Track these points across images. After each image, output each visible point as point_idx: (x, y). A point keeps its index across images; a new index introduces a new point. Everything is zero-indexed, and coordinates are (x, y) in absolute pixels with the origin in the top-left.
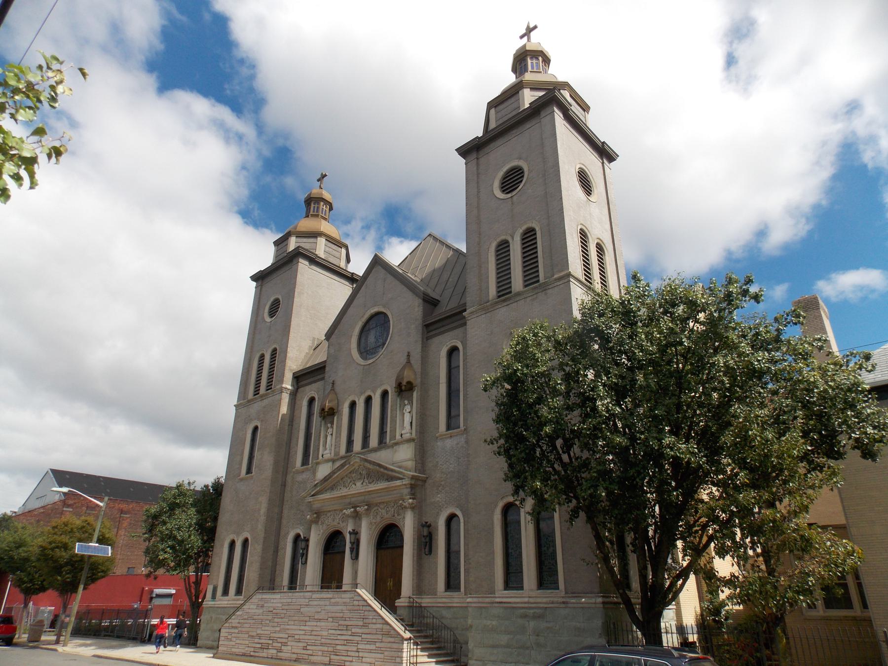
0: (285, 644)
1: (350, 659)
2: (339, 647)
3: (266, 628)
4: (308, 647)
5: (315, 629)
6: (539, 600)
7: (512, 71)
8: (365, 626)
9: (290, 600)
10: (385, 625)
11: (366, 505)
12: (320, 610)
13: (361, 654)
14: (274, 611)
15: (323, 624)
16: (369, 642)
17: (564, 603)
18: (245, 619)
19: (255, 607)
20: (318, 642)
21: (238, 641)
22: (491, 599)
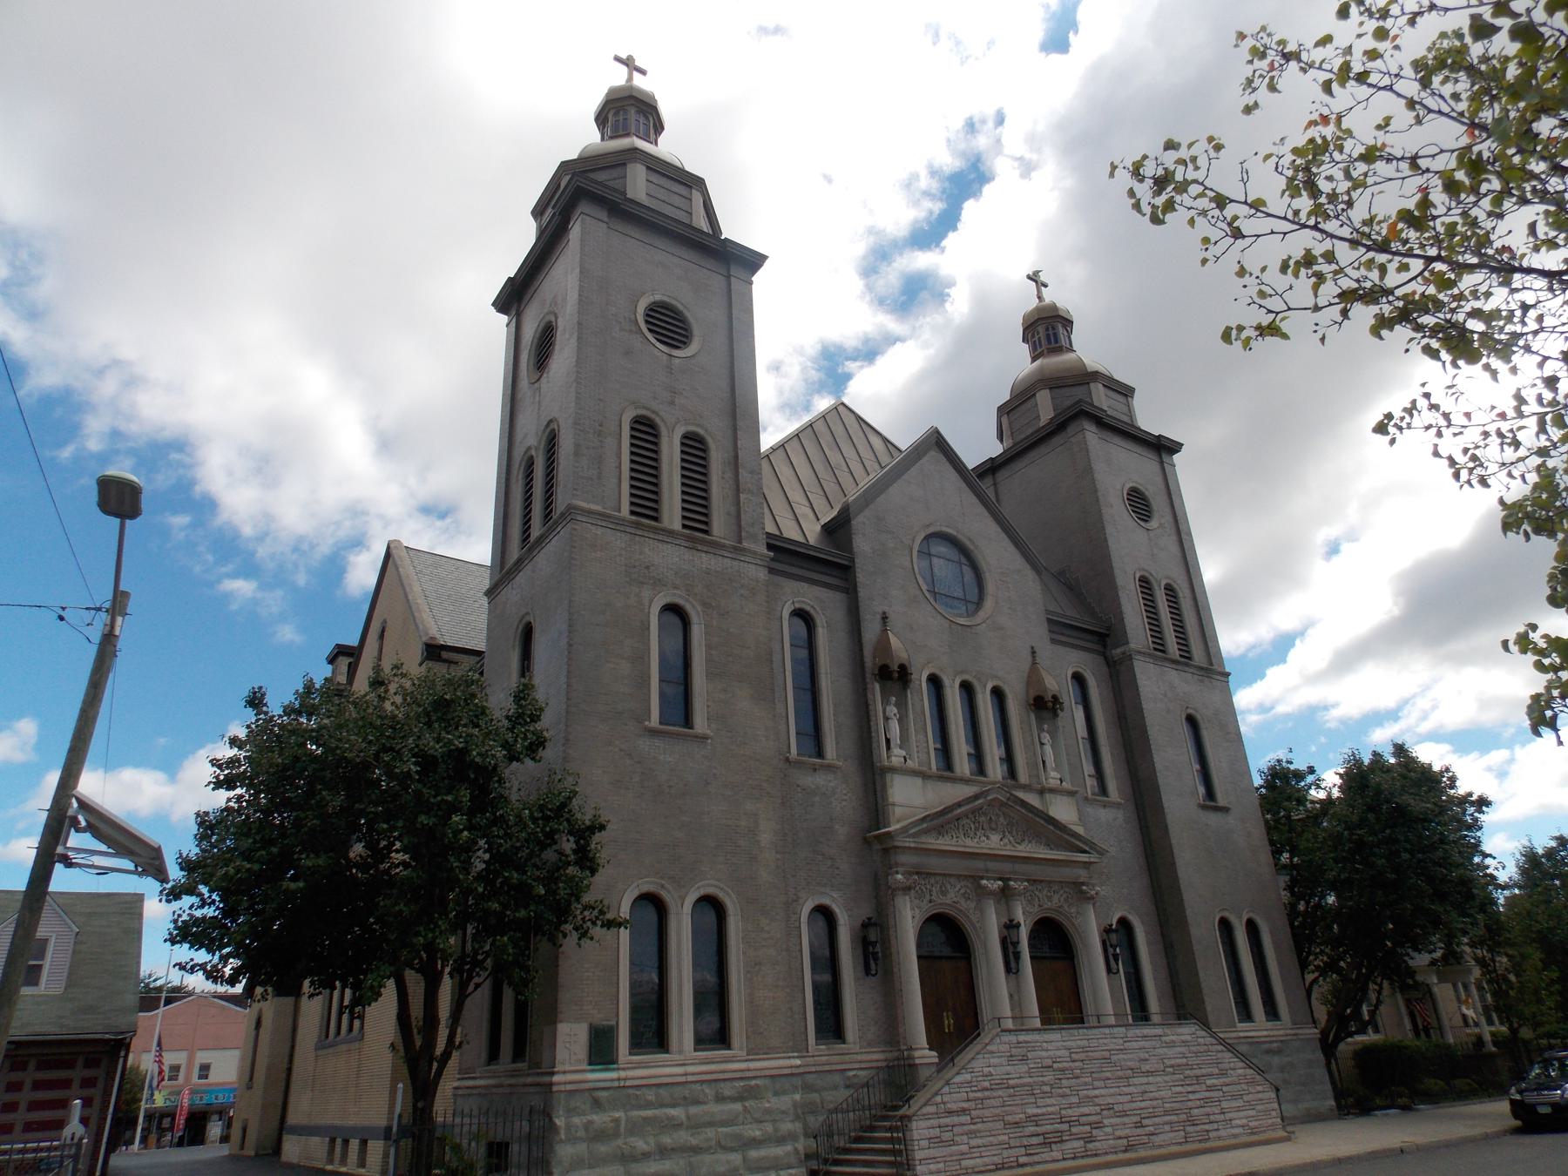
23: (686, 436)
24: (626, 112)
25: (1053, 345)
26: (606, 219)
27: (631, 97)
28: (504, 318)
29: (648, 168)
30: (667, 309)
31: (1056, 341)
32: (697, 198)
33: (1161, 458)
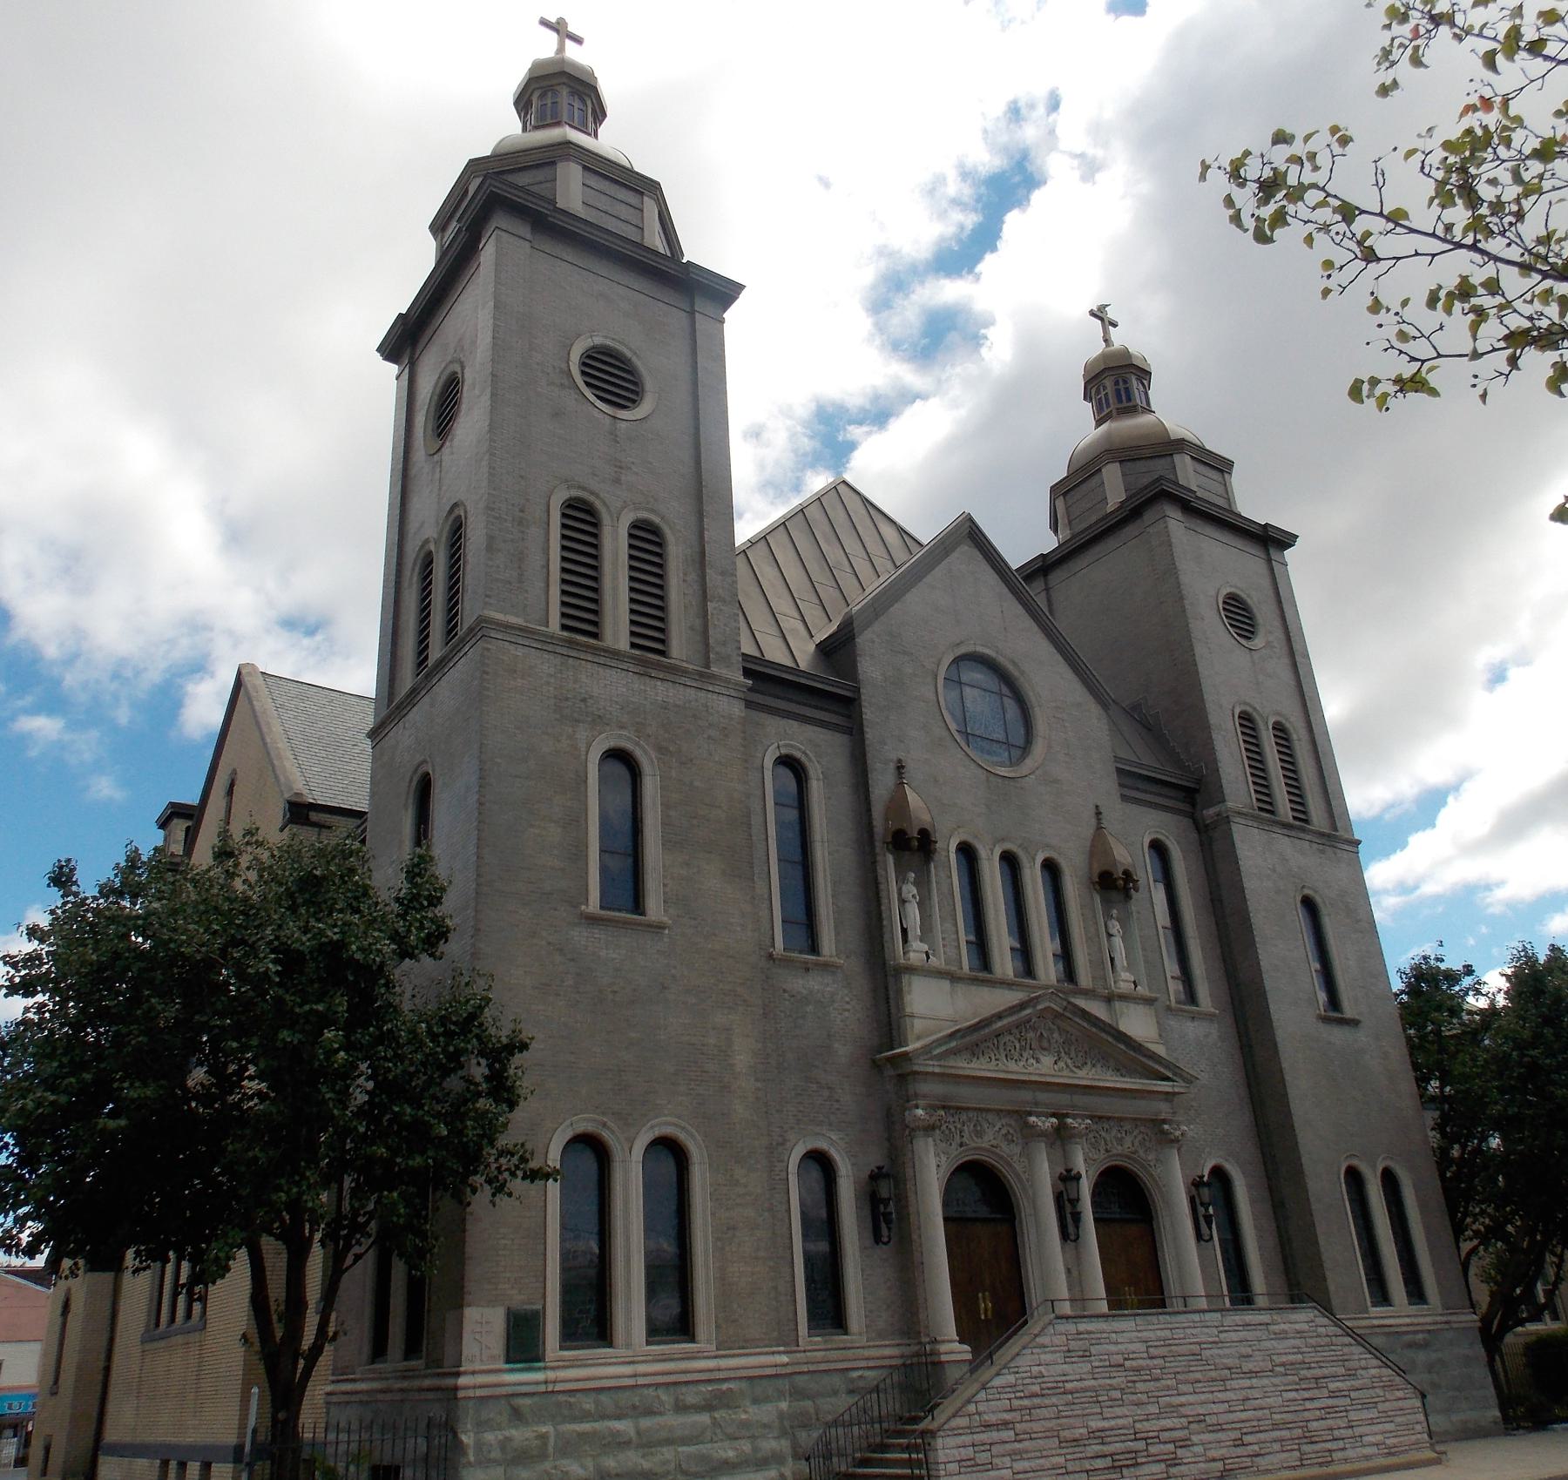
0: (1184, 1443)
1: (1341, 1444)
2: (1314, 1425)
3: (1119, 1411)
4: (1247, 1439)
5: (1251, 1393)
6: (1421, 1320)
7: (516, 103)
8: (1351, 1374)
9: (1168, 1333)
10: (1383, 1369)
11: (1054, 1115)
12: (1249, 1351)
13: (1358, 1431)
14: (1128, 1363)
15: (1265, 1381)
16: (1366, 1406)
17: (1446, 1323)
18: (1035, 1395)
19: (1059, 1357)
20: (1267, 1422)
21: (1019, 1466)
22: (1459, 1320)
25: (1125, 404)
26: (529, 236)
27: (563, 73)
29: (585, 168)
30: (611, 356)
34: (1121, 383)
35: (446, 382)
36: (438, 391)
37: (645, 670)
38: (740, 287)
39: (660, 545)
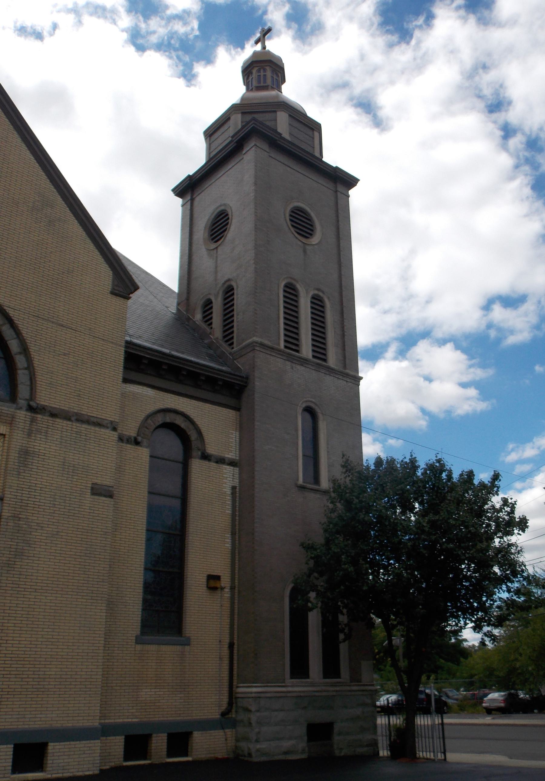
23: (286, 286)
24: (265, 70)
25: (262, 84)
26: (268, 150)
27: (270, 61)
28: (179, 201)
29: (290, 116)
30: (302, 212)
31: (265, 81)
32: (316, 134)
33: (336, 187)
34: (262, 75)
35: (218, 213)
36: (213, 217)
37: (290, 358)
38: (358, 180)
39: (296, 296)
